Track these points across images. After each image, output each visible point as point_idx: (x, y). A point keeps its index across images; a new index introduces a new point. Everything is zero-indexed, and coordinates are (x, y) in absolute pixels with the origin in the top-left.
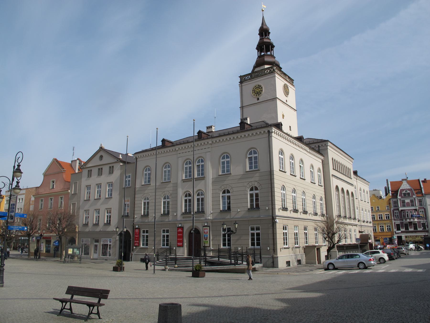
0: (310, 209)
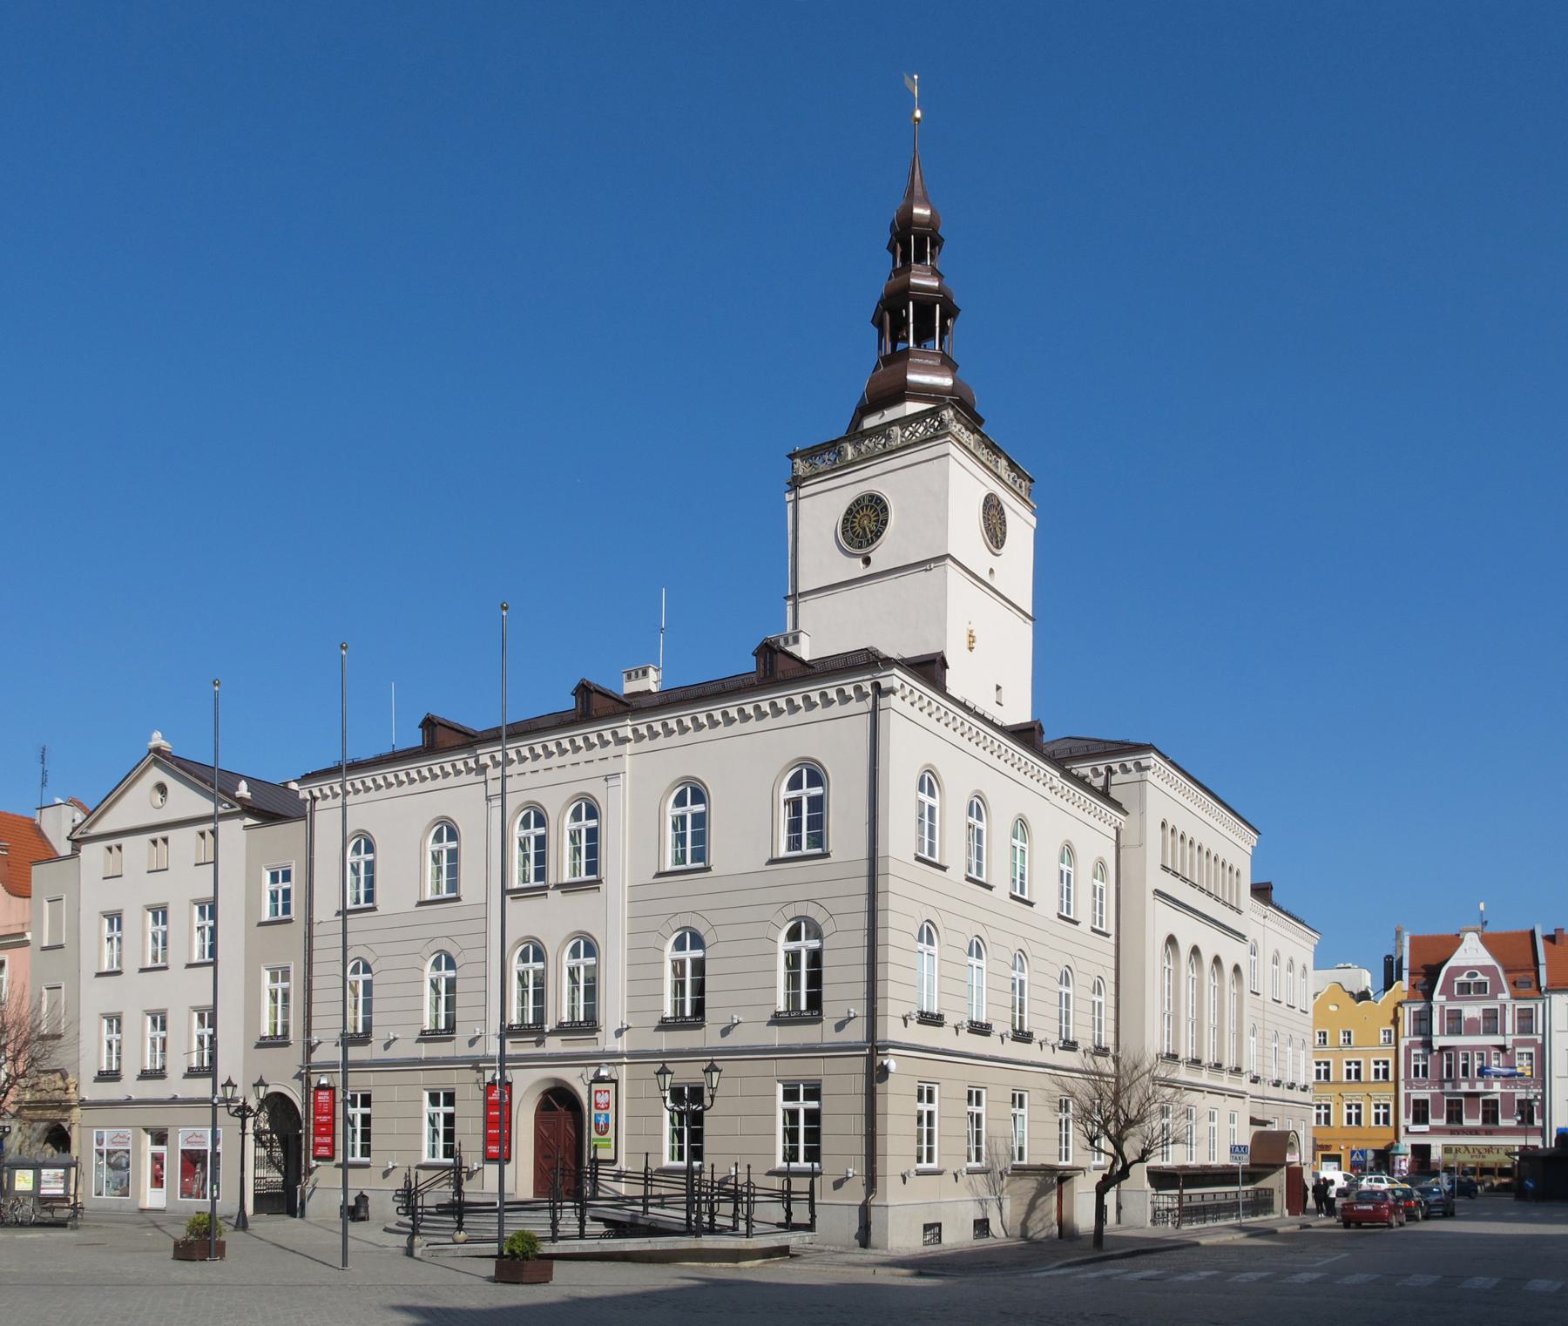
0: (1043, 1024)
